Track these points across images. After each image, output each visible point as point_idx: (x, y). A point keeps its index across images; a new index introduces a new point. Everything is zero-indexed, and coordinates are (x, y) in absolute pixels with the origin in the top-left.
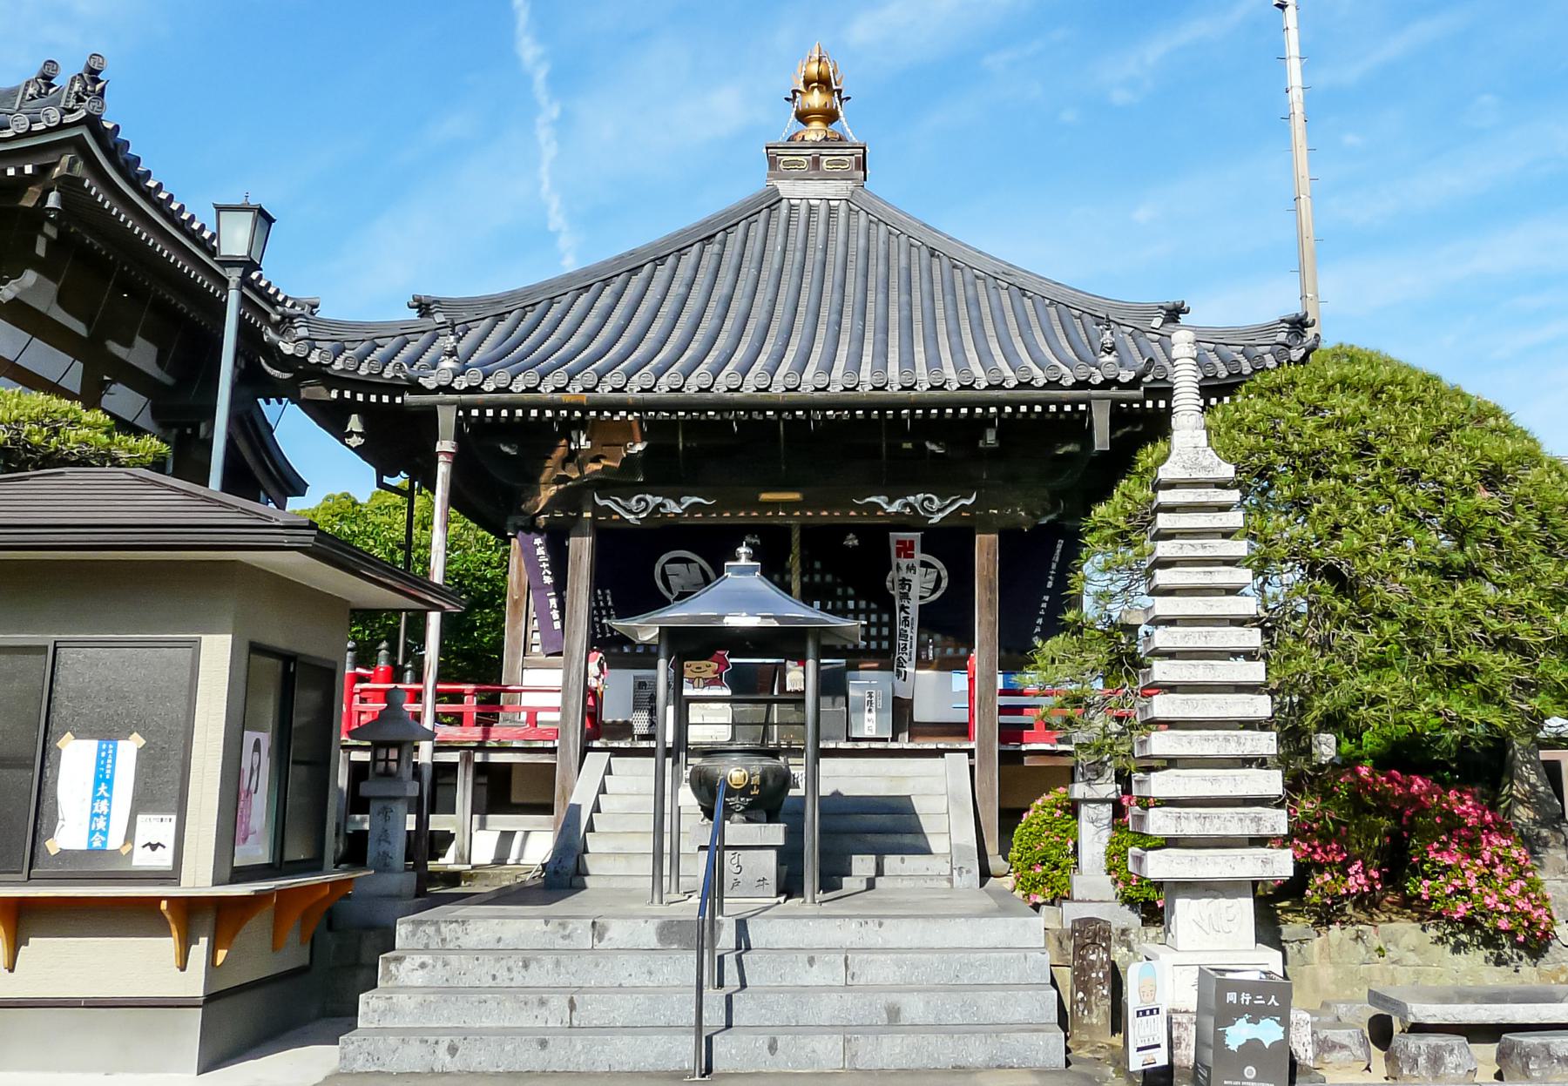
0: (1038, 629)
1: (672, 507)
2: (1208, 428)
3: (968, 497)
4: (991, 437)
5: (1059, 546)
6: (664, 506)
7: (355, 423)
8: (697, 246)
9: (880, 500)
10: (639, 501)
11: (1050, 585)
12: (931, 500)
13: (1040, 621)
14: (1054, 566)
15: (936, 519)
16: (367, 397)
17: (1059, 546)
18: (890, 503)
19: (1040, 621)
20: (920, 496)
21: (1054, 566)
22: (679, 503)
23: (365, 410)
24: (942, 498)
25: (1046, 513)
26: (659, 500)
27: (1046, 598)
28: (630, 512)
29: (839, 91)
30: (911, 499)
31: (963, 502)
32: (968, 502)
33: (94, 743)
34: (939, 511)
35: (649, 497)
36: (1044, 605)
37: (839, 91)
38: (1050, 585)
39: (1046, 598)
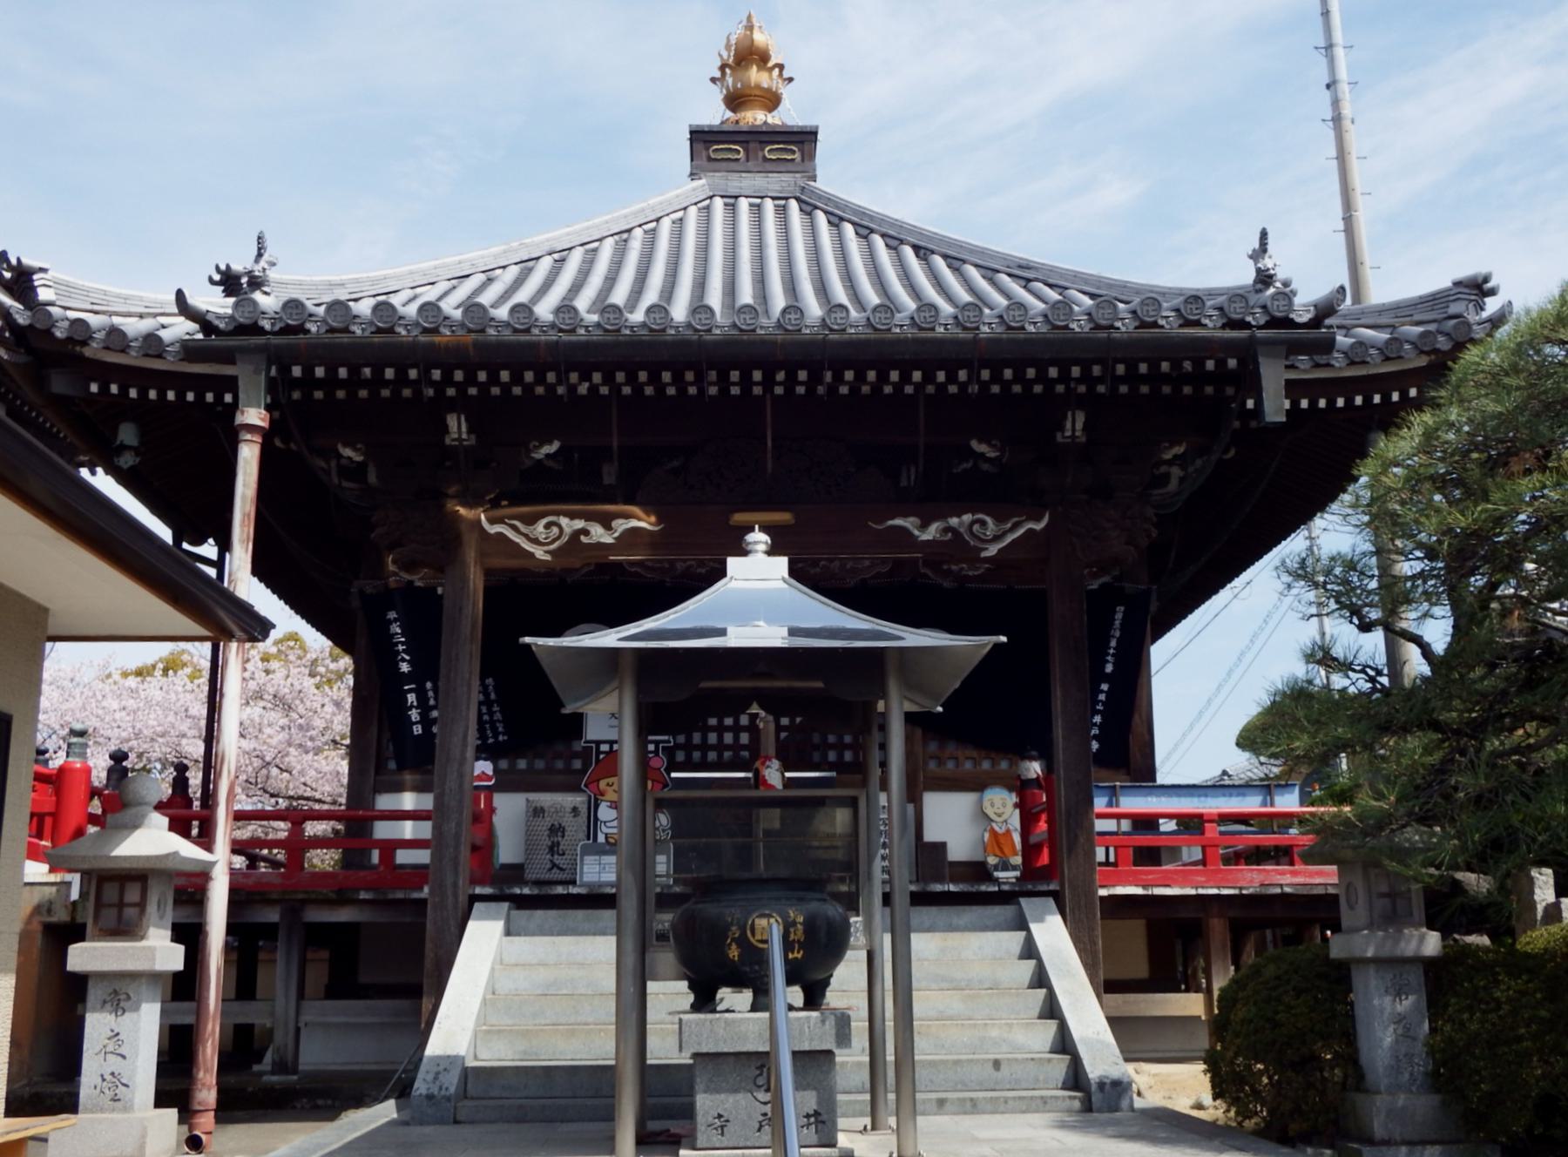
0: (1095, 731)
1: (598, 534)
2: (1519, 345)
3: (1038, 519)
4: (1075, 425)
5: (1119, 616)
6: (586, 532)
7: (127, 434)
8: (610, 242)
9: (908, 523)
10: (547, 526)
11: (1109, 668)
12: (983, 523)
13: (1098, 719)
14: (1113, 643)
15: (992, 550)
16: (143, 393)
17: (1119, 616)
18: (924, 526)
19: (1098, 719)
20: (967, 518)
21: (1113, 643)
22: (608, 527)
23: (140, 412)
24: (999, 519)
25: (1095, 576)
26: (579, 524)
27: (1105, 687)
28: (536, 541)
29: (781, 67)
30: (954, 521)
31: (1031, 525)
32: (1039, 526)
33: (914, 936)
34: (996, 538)
35: (564, 521)
36: (1102, 697)
37: (781, 67)
38: (1109, 668)
39: (1105, 687)
